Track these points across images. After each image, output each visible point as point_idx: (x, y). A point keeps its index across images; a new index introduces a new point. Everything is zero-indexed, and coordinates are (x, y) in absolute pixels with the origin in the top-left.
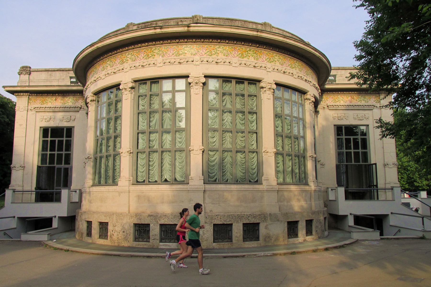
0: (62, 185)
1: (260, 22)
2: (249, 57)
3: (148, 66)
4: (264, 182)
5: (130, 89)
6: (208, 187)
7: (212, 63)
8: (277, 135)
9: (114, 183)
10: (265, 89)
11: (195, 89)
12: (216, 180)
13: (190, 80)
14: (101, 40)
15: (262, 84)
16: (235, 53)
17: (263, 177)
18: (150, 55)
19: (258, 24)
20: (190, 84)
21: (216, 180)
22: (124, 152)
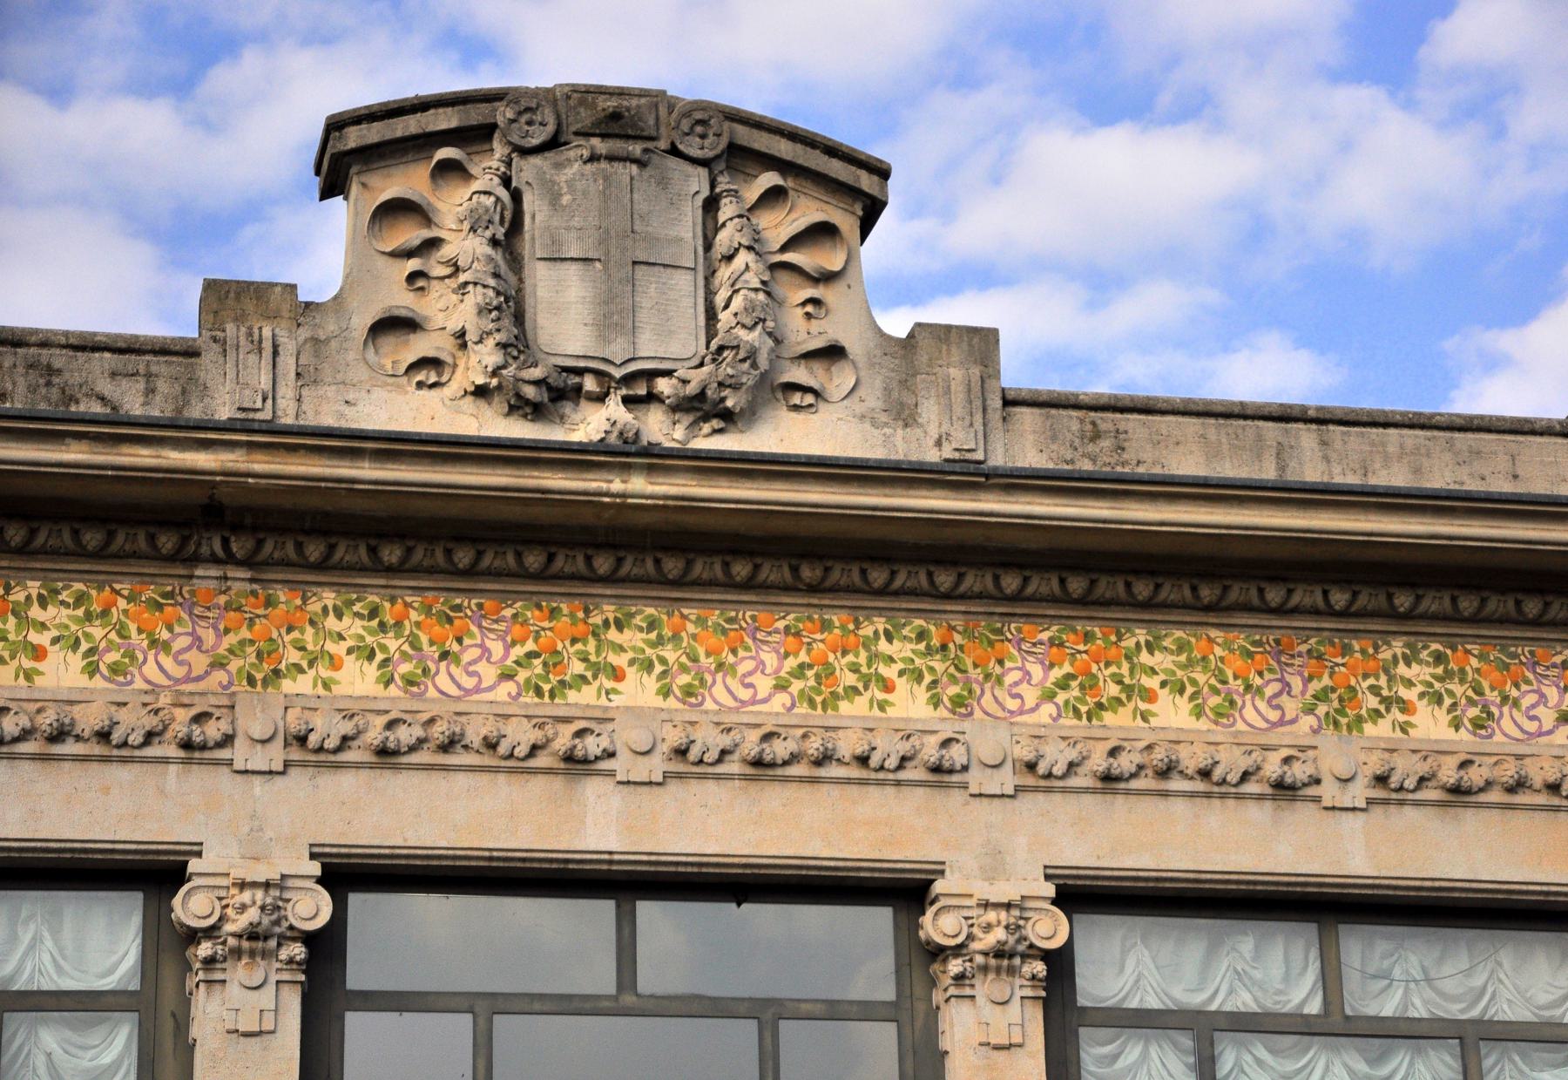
13: (191, 907)
16: (197, 642)
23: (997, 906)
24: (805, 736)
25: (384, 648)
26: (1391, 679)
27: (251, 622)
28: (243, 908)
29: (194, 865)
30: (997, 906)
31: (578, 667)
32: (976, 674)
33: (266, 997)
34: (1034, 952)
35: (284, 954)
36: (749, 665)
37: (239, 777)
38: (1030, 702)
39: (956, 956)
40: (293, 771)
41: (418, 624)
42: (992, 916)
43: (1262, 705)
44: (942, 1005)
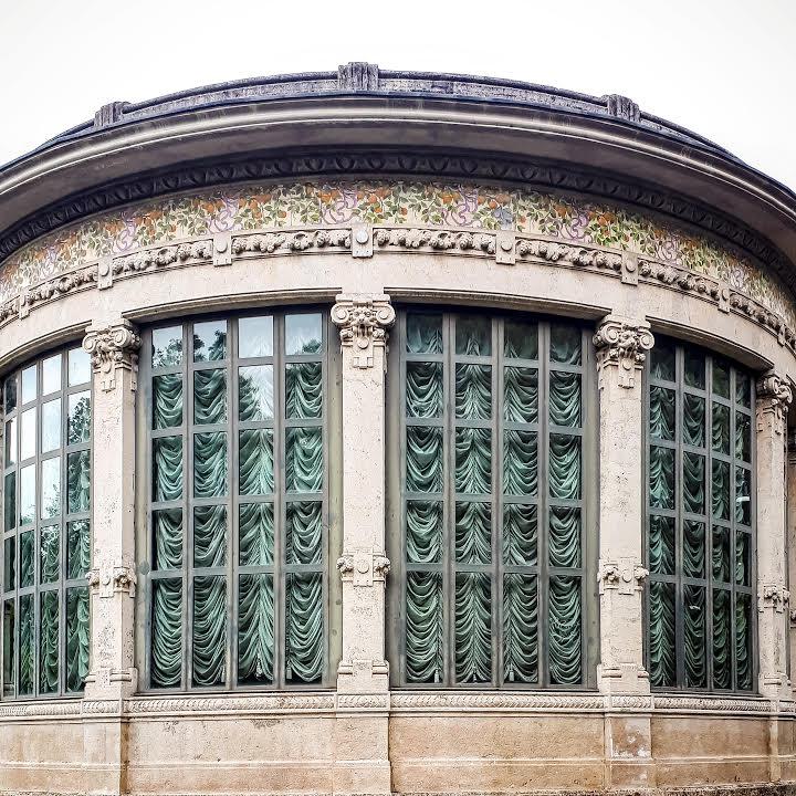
0: (359, 624)
1: (332, 68)
2: (522, 220)
3: (178, 263)
4: (604, 684)
5: (119, 355)
6: (404, 699)
7: (422, 249)
8: (658, 528)
9: (75, 684)
10: (613, 352)
11: (355, 347)
12: (431, 679)
13: (338, 314)
14: (44, 153)
15: (605, 333)
16: (467, 209)
17: (599, 667)
18: (387, 209)
19: (323, 78)
20: (339, 328)
21: (431, 679)
22: (103, 580)
23: (362, 305)
24: (596, 254)
25: (424, 205)
26: (396, 197)
27: (489, 201)
28: (627, 337)
29: (338, 297)
30: (362, 305)
31: (613, 234)
32: (445, 207)
33: (369, 353)
34: (380, 326)
35: (375, 333)
36: (463, 208)
37: (359, 261)
38: (469, 219)
39: (612, 348)
40: (376, 256)
41: (439, 195)
42: (628, 332)
43: (456, 217)
44: (602, 369)
